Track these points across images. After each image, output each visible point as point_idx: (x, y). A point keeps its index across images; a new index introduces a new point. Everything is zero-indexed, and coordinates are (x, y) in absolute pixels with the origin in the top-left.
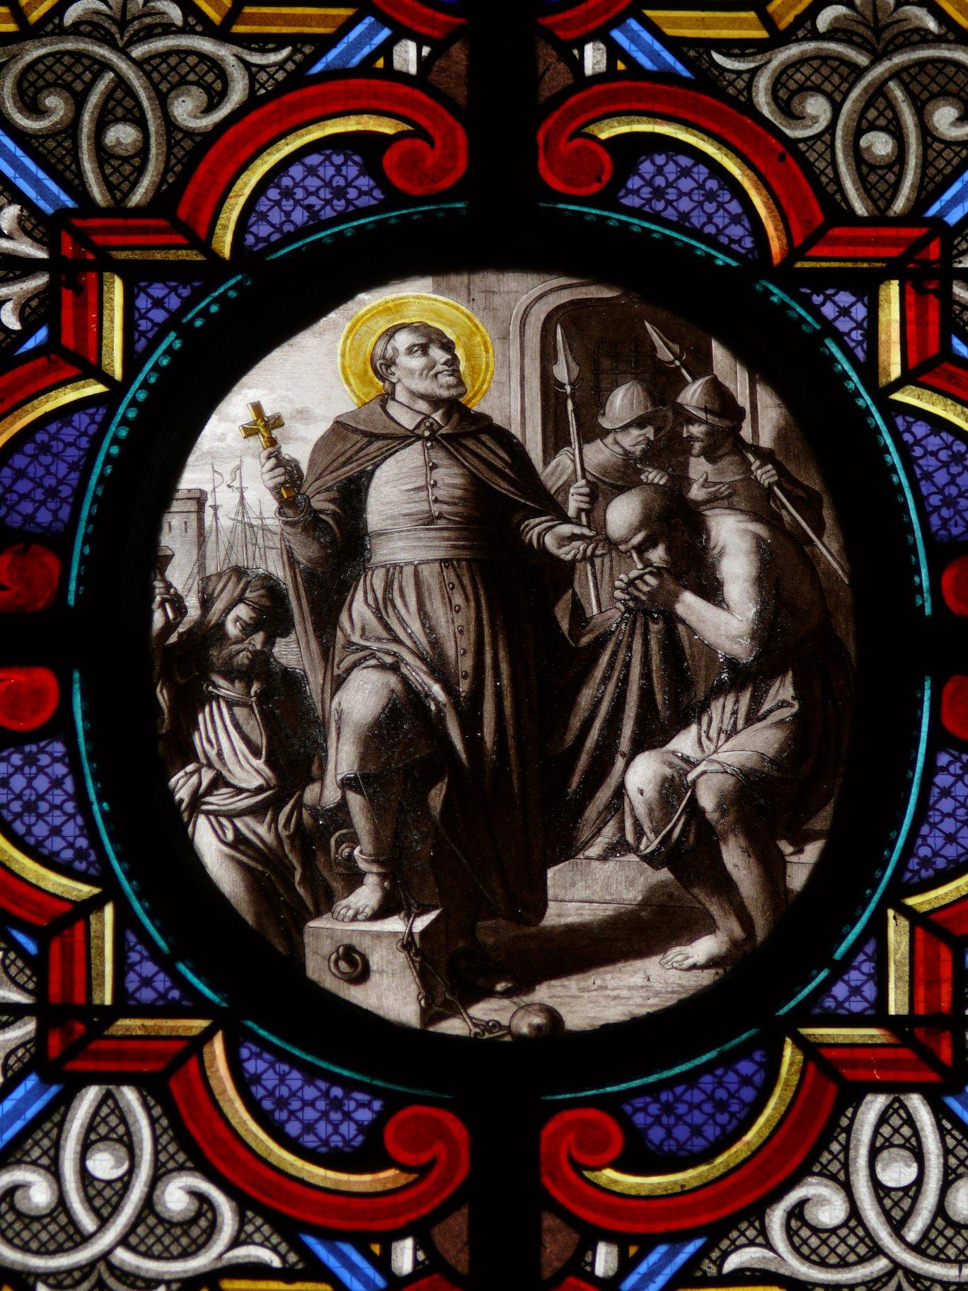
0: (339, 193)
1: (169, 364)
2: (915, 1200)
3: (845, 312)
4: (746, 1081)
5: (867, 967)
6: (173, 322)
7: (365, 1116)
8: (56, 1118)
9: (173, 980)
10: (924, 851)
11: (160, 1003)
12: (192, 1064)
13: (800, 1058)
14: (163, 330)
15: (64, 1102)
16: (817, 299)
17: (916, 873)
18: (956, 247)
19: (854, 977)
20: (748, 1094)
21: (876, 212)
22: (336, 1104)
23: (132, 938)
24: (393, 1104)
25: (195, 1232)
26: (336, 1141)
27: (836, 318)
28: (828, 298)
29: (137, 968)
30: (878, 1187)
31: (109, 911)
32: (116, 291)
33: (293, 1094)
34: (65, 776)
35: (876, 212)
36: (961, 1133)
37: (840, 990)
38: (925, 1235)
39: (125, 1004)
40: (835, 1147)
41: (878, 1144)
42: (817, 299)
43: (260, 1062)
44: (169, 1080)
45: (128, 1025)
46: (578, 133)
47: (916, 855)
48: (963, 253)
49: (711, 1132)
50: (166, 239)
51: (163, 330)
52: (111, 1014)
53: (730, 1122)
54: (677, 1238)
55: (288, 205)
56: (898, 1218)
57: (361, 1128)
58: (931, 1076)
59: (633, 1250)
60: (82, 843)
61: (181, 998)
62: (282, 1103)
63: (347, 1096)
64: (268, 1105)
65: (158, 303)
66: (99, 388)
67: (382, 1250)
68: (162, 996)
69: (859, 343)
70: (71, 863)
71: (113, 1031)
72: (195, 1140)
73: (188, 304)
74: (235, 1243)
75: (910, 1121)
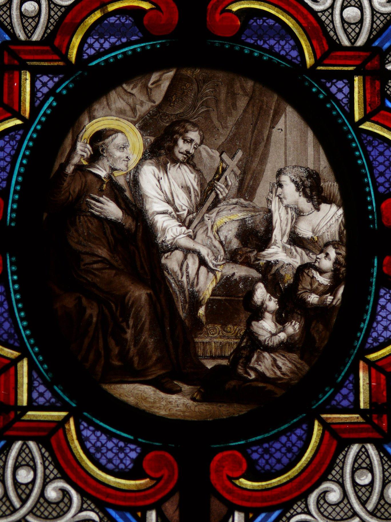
0: (266, 451)
1: (51, 112)
2: (353, 467)
3: (340, 90)
4: (91, 46)
5: (39, 95)
6: (52, 92)
7: (133, 455)
8: (374, 33)
9: (329, 90)
10: (374, 335)
11: (47, 404)
12: (319, 56)
13: (321, 428)
14: (46, 97)
15: (370, 41)
16: (328, 85)
17: (372, 344)
18: (387, 59)
19: (344, 391)
20: (300, 444)
21: (27, 442)
22: (121, 450)
23: (35, 375)
24: (145, 449)
25: (62, 505)
26: (122, 466)
27: (45, 391)
28: (333, 84)
29: (37, 388)
30: (355, 484)
31: (25, 362)
32: (27, 76)
33: (103, 445)
34: (378, 177)
35: (27, 442)
36: (4, 24)
37: (338, 397)
38: (376, 507)
39: (32, 406)
40: (337, 469)
41: (37, 18)
42: (328, 85)
43: (88, 431)
44: (49, 437)
45: (31, 414)
46: (158, 480)
47: (371, 336)
48: (389, 62)
49: (285, 461)
50: (50, 57)
51: (46, 97)
52: (25, 410)
53: (293, 456)
54: (270, 510)
55: (289, 444)
56: (364, 500)
57: (132, 460)
58: (376, 435)
59: (251, 515)
60: (369, 149)
61: (325, 83)
62: (98, 450)
63: (126, 446)
64: (92, 450)
65: (44, 84)
66: (19, 122)
67: (142, 514)
68: (48, 401)
69: (346, 104)
70: (7, 341)
71: (25, 418)
72: (65, 466)
73: (332, 397)
74: (81, 510)
75: (24, 28)
